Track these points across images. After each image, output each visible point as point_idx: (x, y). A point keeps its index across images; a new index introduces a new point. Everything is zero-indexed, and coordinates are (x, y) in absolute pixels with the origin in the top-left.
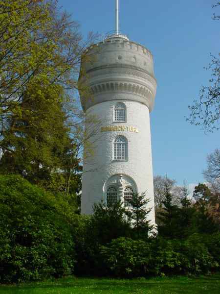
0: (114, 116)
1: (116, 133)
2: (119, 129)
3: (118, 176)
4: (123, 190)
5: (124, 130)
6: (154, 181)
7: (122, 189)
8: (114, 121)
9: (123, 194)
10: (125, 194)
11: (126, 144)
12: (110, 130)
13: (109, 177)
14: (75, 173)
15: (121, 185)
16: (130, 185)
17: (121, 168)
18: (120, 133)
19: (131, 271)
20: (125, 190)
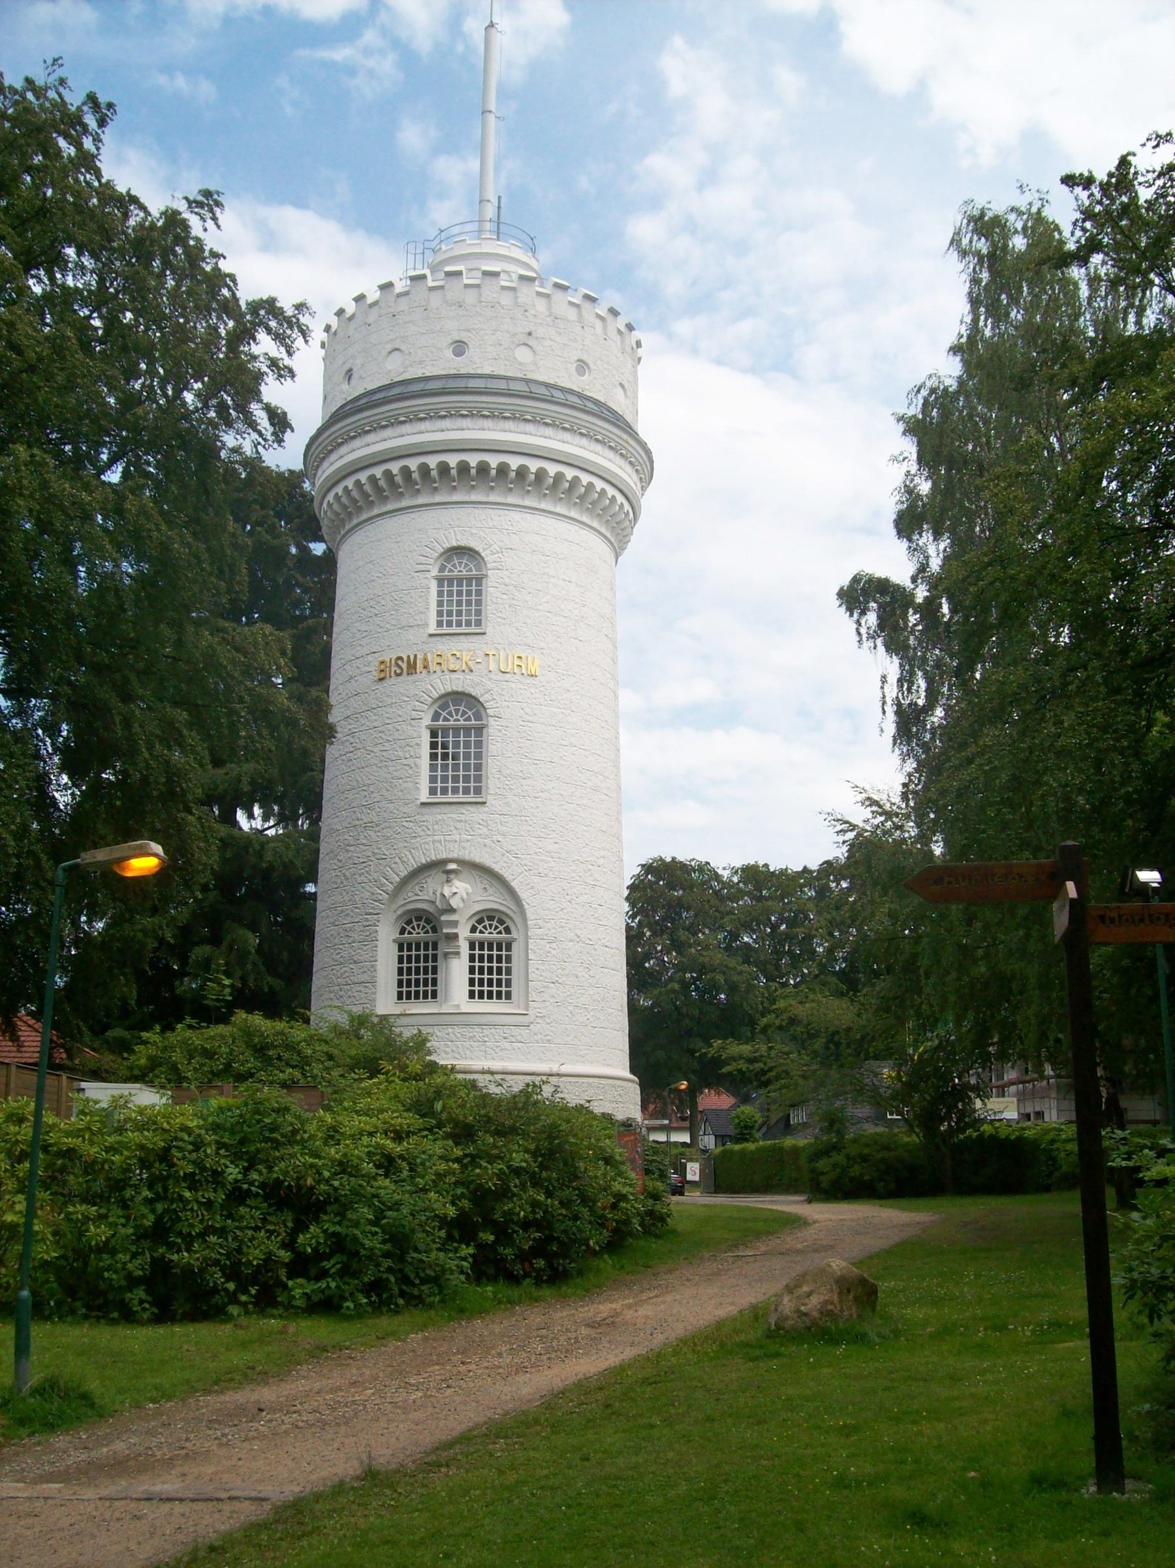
10: (472, 946)
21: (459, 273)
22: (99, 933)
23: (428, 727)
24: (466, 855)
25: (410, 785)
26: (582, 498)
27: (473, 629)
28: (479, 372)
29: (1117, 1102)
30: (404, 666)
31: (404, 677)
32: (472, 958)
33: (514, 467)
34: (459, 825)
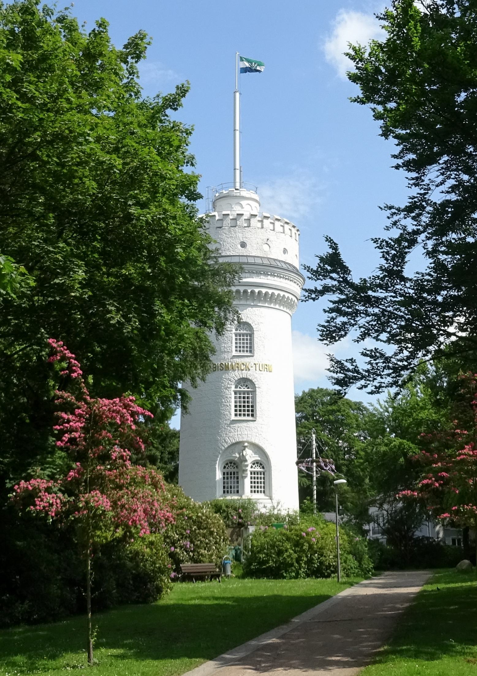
0: (234, 345)
1: (236, 375)
2: (243, 367)
3: (239, 445)
4: (249, 468)
5: (249, 370)
6: (297, 404)
7: (247, 466)
8: (234, 353)
9: (249, 473)
10: (251, 474)
11: (251, 335)
12: (226, 368)
13: (226, 446)
14: (75, 314)
15: (246, 461)
16: (259, 459)
17: (246, 432)
18: (245, 374)
19: (101, 367)
20: (252, 467)
21: (228, 215)
22: (14, 365)
23: (234, 391)
24: (253, 441)
25: (228, 413)
26: (271, 298)
27: (248, 354)
28: (251, 255)
29: (468, 531)
30: (223, 367)
31: (223, 371)
32: (251, 478)
33: (264, 292)
34: (247, 428)
